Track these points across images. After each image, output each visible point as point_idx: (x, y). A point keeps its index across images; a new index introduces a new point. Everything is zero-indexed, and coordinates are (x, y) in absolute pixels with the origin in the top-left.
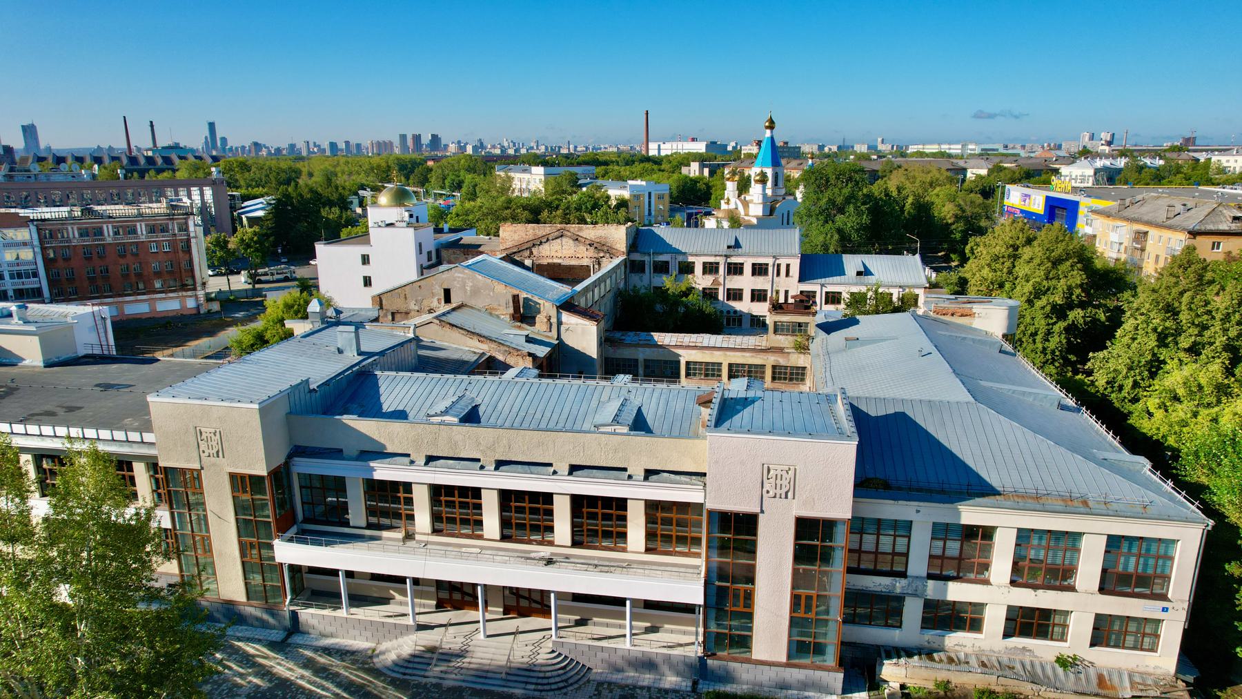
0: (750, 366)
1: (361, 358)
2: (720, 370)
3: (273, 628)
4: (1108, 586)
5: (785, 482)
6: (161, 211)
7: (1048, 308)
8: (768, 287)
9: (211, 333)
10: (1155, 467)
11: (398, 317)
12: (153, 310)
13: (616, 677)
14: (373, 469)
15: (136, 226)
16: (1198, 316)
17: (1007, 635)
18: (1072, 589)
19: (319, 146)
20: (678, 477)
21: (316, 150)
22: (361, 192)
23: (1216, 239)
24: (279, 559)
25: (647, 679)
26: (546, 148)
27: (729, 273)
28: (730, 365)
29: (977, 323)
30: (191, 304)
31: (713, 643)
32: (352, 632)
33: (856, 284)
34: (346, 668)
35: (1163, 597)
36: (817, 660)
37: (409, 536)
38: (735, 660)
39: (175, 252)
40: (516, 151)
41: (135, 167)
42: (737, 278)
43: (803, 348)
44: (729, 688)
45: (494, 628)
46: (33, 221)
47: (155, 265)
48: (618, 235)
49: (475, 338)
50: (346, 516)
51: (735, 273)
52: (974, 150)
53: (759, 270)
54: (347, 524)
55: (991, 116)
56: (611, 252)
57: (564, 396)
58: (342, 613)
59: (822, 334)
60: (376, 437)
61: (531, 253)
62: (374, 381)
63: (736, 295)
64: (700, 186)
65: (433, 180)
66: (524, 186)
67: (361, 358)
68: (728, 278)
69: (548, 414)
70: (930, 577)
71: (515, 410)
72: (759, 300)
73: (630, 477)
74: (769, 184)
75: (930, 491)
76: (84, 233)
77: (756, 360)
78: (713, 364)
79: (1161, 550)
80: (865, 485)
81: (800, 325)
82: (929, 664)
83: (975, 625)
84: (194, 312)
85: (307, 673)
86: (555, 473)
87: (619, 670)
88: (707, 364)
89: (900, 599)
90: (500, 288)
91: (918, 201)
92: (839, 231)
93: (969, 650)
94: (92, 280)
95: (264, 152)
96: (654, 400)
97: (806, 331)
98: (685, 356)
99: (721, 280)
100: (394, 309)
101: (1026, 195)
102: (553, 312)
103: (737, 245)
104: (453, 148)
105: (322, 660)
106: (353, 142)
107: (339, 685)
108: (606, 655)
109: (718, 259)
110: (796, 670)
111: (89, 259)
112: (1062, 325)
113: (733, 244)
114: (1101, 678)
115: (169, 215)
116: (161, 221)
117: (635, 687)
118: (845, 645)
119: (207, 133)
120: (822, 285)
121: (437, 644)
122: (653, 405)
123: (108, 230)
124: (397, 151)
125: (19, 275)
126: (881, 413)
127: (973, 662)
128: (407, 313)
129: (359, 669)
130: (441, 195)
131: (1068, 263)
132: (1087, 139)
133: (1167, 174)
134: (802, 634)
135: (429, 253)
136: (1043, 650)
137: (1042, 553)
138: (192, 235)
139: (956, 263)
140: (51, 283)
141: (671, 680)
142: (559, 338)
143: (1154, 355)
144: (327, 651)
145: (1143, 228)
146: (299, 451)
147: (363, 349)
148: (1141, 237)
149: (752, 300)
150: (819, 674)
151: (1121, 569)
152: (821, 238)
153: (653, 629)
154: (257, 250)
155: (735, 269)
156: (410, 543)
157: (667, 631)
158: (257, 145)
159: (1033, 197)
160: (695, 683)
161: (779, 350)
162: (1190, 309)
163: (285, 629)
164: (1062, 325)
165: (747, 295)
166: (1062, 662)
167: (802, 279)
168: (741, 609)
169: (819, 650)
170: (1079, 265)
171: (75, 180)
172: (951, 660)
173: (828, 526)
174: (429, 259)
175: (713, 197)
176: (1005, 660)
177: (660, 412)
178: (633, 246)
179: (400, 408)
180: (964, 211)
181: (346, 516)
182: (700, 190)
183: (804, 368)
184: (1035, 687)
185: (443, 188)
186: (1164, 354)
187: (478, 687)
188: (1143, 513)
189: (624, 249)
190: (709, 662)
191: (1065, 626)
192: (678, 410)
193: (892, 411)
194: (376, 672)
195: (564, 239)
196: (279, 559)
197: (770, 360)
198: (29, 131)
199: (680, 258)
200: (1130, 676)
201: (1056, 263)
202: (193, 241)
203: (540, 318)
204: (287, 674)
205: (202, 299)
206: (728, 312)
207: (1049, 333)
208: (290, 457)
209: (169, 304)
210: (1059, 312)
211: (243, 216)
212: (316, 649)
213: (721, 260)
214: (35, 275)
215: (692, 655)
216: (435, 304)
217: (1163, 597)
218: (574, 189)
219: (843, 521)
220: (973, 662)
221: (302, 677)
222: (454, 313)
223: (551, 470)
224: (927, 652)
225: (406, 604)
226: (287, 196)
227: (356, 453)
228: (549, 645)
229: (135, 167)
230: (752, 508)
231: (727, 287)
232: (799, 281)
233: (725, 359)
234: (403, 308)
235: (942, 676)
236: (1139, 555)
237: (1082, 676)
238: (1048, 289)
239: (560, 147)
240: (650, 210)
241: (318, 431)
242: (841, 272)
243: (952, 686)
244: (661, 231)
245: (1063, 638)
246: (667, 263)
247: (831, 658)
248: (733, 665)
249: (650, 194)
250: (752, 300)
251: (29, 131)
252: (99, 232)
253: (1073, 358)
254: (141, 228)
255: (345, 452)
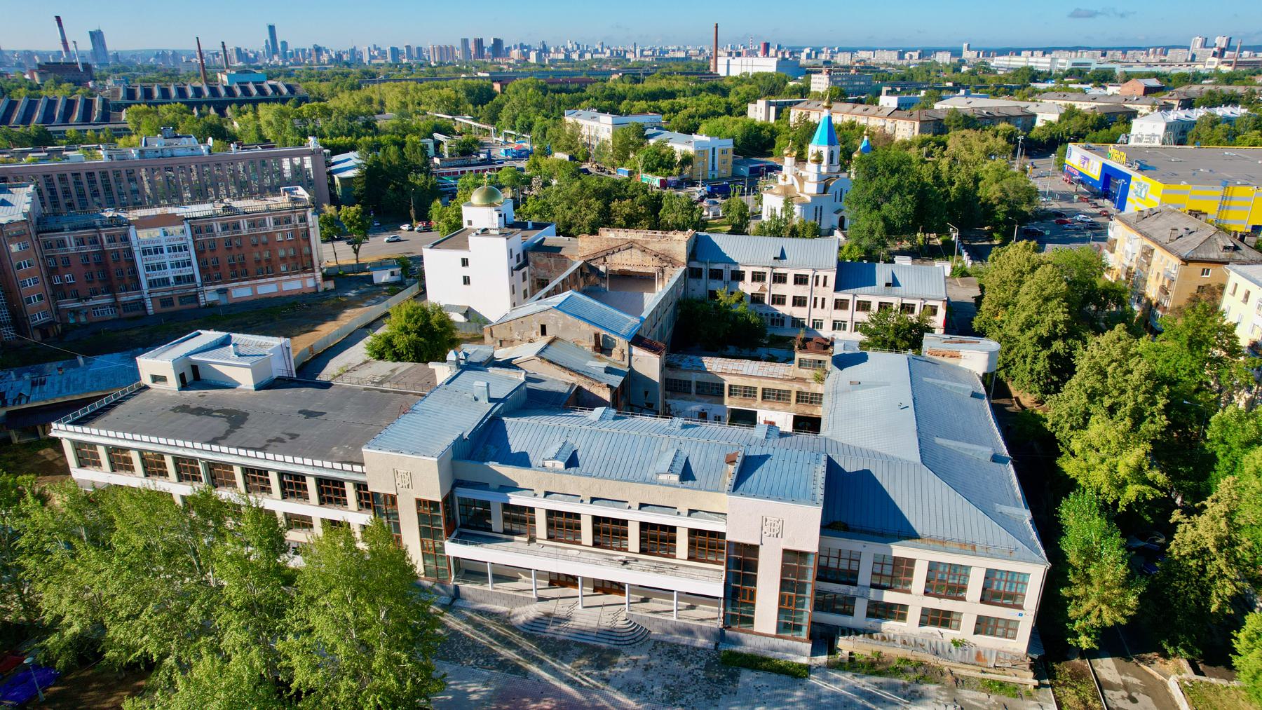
0: (779, 391)
1: (491, 405)
2: (755, 392)
3: (443, 595)
4: (987, 598)
5: (776, 528)
6: (285, 205)
7: (1035, 339)
8: (807, 294)
9: (334, 317)
10: (1037, 522)
11: (504, 343)
12: (280, 290)
13: (667, 638)
14: (509, 498)
15: (265, 220)
16: (1118, 382)
17: (920, 625)
18: (963, 599)
19: (379, 49)
20: (709, 515)
21: (376, 53)
22: (439, 137)
23: (1206, 266)
24: (447, 553)
25: (686, 640)
26: (612, 53)
27: (774, 281)
28: (764, 389)
29: (963, 364)
30: (310, 283)
31: (729, 621)
32: (494, 600)
33: (884, 295)
34: (494, 624)
35: (1020, 607)
36: (796, 634)
37: (532, 540)
38: (743, 631)
39: (297, 240)
40: (580, 56)
41: (217, 99)
42: (781, 286)
43: (820, 380)
44: (738, 649)
45: (588, 601)
46: (187, 219)
47: (282, 253)
48: (678, 243)
49: (567, 372)
50: (488, 521)
51: (780, 282)
52: (1064, 64)
53: (800, 280)
54: (490, 530)
55: (1091, 15)
56: (673, 263)
57: (635, 445)
58: (489, 587)
59: (836, 371)
60: (512, 478)
61: (605, 261)
62: (503, 424)
63: (779, 300)
64: (765, 133)
65: (504, 120)
66: (592, 134)
67: (491, 405)
68: (774, 286)
69: (624, 460)
70: (873, 586)
71: (602, 455)
72: (800, 305)
73: (679, 513)
74: (825, 162)
75: (873, 533)
76: (225, 228)
77: (785, 386)
78: (750, 388)
79: (1021, 579)
80: (828, 527)
81: (820, 362)
82: (869, 640)
83: (902, 617)
84: (314, 290)
85: (469, 627)
86: (630, 507)
87: (668, 633)
88: (746, 387)
89: (853, 599)
90: (585, 326)
91: (964, 188)
92: (885, 219)
93: (897, 632)
94: (232, 266)
95: (325, 58)
96: (698, 452)
97: (824, 367)
98: (729, 381)
99: (767, 287)
100: (502, 337)
101: (1086, 158)
102: (626, 347)
103: (783, 256)
104: (515, 54)
105: (478, 618)
106: (414, 46)
107: (491, 636)
108: (660, 624)
109: (765, 270)
110: (781, 640)
111: (230, 249)
112: (1045, 353)
113: (779, 256)
114: (979, 654)
115: (290, 209)
116: (286, 214)
117: (678, 645)
118: (813, 624)
119: (268, 37)
120: (854, 295)
121: (552, 611)
122: (697, 455)
123: (244, 224)
124: (458, 54)
125: (178, 265)
126: (853, 470)
127: (898, 641)
128: (512, 342)
129: (502, 626)
130: (511, 135)
131: (1055, 302)
132: (1198, 45)
133: (1242, 129)
134: (786, 618)
135: (518, 256)
136: (949, 634)
137: (946, 576)
138: (310, 225)
139: (996, 242)
140: (202, 270)
141: (701, 642)
142: (630, 366)
143: (1087, 409)
144: (480, 612)
145: (1153, 245)
146: (458, 483)
147: (493, 396)
148: (1147, 253)
149: (794, 305)
150: (799, 644)
151: (995, 588)
152: (867, 224)
153: (692, 607)
154: (359, 228)
155: (780, 278)
156: (533, 545)
157: (701, 609)
158: (318, 50)
159: (1091, 161)
160: (717, 644)
161: (803, 380)
162: (1114, 377)
163: (450, 596)
164: (1045, 353)
165: (789, 301)
166: (955, 643)
167: (837, 289)
168: (747, 601)
169: (798, 628)
170: (1065, 304)
171: (194, 152)
172: (884, 638)
173: (803, 555)
174: (518, 261)
175: (777, 145)
176: (919, 641)
177: (701, 462)
178: (692, 255)
179: (523, 450)
180: (1007, 196)
181: (488, 521)
182: (764, 138)
183: (821, 395)
184: (935, 658)
185: (513, 128)
186: (1092, 409)
187: (579, 641)
188: (1009, 555)
189: (685, 261)
190: (727, 632)
191: (959, 621)
192: (714, 461)
193: (860, 469)
194: (514, 628)
195: (633, 250)
196: (447, 553)
197: (795, 387)
198: (96, 37)
199: (733, 268)
200: (997, 654)
201: (1047, 300)
202: (311, 230)
203: (616, 351)
204: (458, 627)
205: (319, 279)
206: (772, 315)
207: (1035, 358)
208: (454, 487)
209: (293, 284)
210: (1045, 342)
211: (335, 176)
212: (472, 611)
213: (768, 271)
214: (189, 264)
215: (715, 626)
216: (533, 335)
217: (1020, 607)
218: (641, 140)
219: (813, 553)
220: (898, 641)
221: (467, 630)
222: (550, 347)
223: (627, 505)
224: (869, 633)
225: (531, 582)
226: (378, 163)
227: (497, 487)
228: (624, 615)
229: (217, 99)
230: (755, 542)
231: (772, 293)
232: (835, 291)
233: (760, 385)
234: (509, 338)
235: (876, 648)
236: (1006, 581)
237: (967, 652)
238: (1038, 322)
239: (625, 52)
240: (713, 165)
241: (470, 470)
242: (872, 282)
243: (882, 655)
244: (717, 239)
245: (958, 628)
246: (721, 271)
247: (804, 634)
248: (741, 635)
249: (714, 149)
250: (794, 305)
251: (96, 37)
252: (237, 226)
253: (1055, 378)
254: (270, 221)
255: (491, 486)
